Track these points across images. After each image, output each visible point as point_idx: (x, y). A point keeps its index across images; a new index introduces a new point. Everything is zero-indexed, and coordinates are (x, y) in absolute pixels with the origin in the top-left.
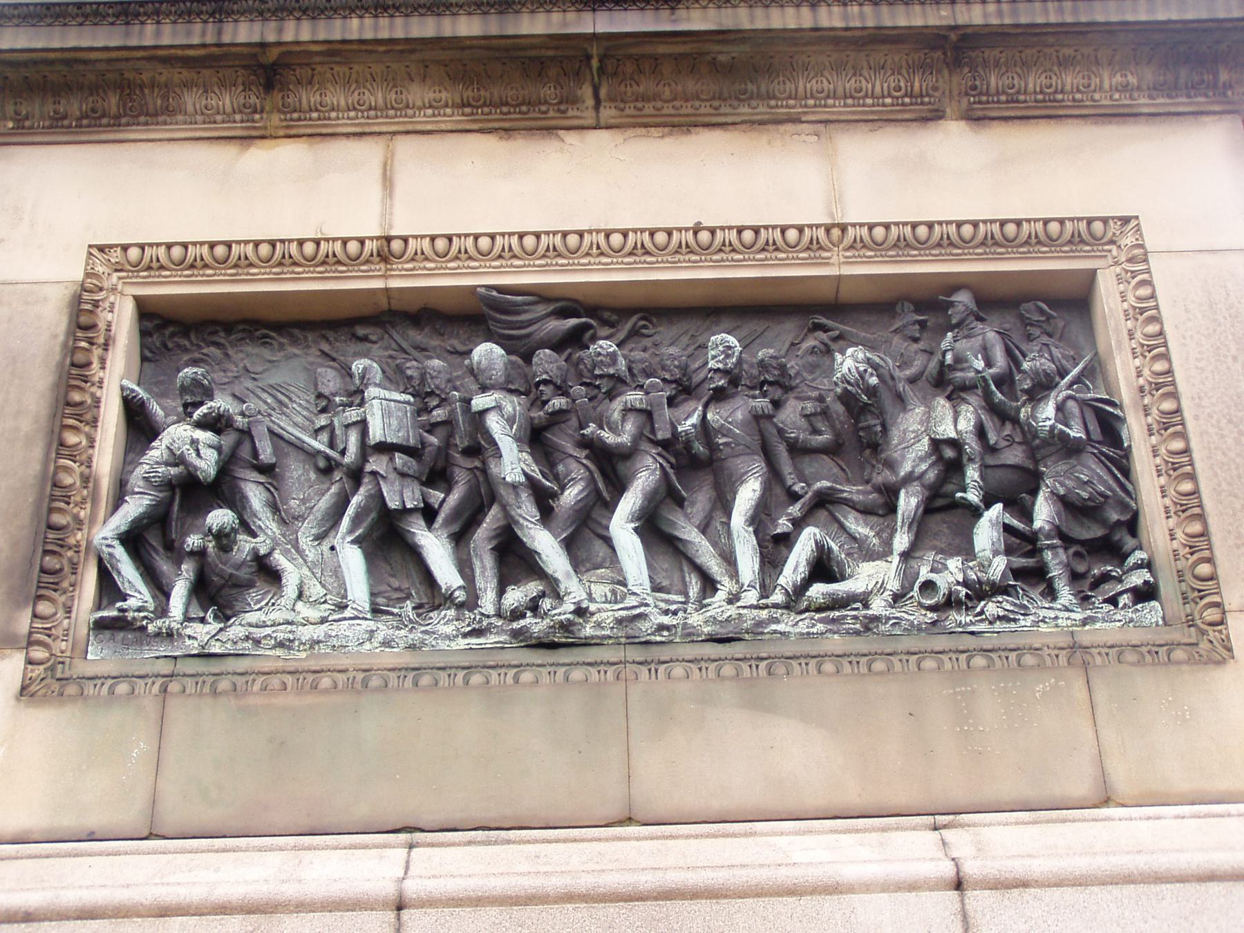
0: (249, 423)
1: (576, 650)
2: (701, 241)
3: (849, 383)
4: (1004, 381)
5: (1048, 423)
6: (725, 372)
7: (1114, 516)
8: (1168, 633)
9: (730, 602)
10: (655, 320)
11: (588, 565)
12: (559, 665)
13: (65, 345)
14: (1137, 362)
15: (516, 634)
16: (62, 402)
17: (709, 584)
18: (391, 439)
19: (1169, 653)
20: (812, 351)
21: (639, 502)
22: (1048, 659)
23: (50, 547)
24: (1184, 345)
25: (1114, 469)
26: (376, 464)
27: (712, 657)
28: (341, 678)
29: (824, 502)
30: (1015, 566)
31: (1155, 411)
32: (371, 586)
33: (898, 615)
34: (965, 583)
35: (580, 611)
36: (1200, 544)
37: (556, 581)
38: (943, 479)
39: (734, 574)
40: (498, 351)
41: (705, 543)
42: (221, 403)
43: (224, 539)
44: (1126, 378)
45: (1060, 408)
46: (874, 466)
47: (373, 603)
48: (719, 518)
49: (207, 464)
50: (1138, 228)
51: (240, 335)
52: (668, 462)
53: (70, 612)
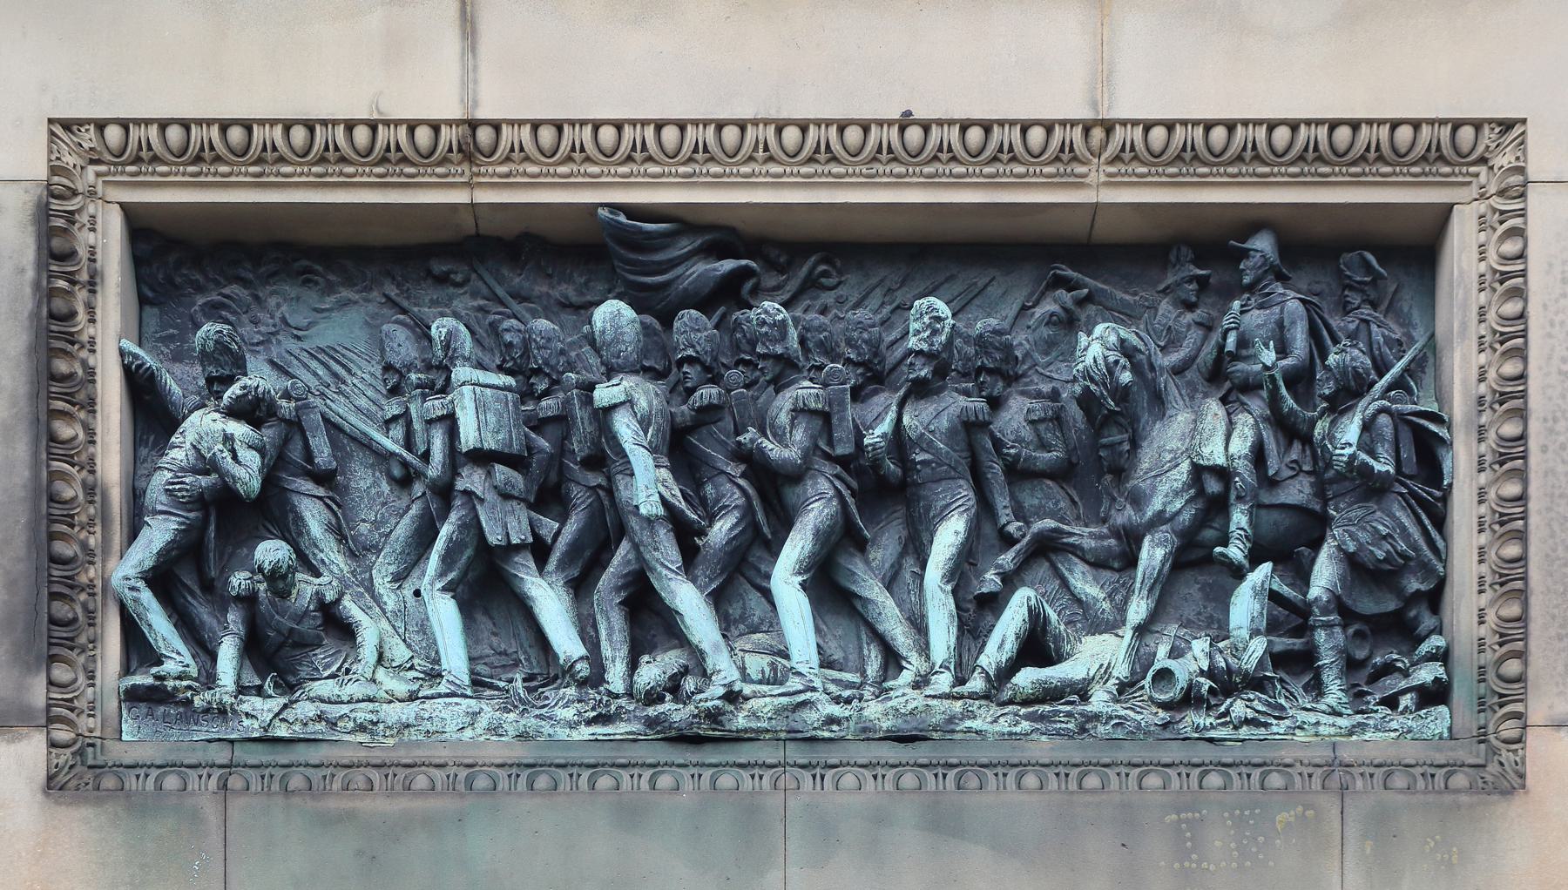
0: (297, 409)
1: (725, 747)
2: (910, 141)
3: (1092, 380)
4: (1300, 380)
5: (1348, 451)
6: (928, 356)
7: (1414, 585)
8: (1452, 749)
9: (916, 686)
10: (839, 264)
11: (742, 627)
12: (703, 765)
13: (37, 285)
14: (1483, 358)
15: (651, 723)
16: (45, 376)
17: (892, 660)
18: (490, 444)
19: (1448, 777)
20: (1051, 320)
21: (809, 547)
22: (1298, 779)
23: (57, 588)
24: (1550, 336)
25: (1424, 517)
26: (472, 479)
27: (891, 761)
28: (439, 774)
29: (1047, 549)
30: (1278, 648)
31: (1492, 435)
32: (468, 647)
33: (1123, 713)
34: (1211, 673)
35: (732, 697)
36: (1513, 636)
37: (702, 652)
38: (1202, 521)
39: (925, 649)
40: (628, 312)
41: (890, 603)
42: (259, 378)
43: (278, 579)
44: (1464, 381)
45: (1367, 427)
46: (1114, 499)
47: (472, 672)
48: (909, 564)
49: (247, 472)
50: (1522, 142)
51: (272, 267)
52: (849, 487)
53: (93, 678)
